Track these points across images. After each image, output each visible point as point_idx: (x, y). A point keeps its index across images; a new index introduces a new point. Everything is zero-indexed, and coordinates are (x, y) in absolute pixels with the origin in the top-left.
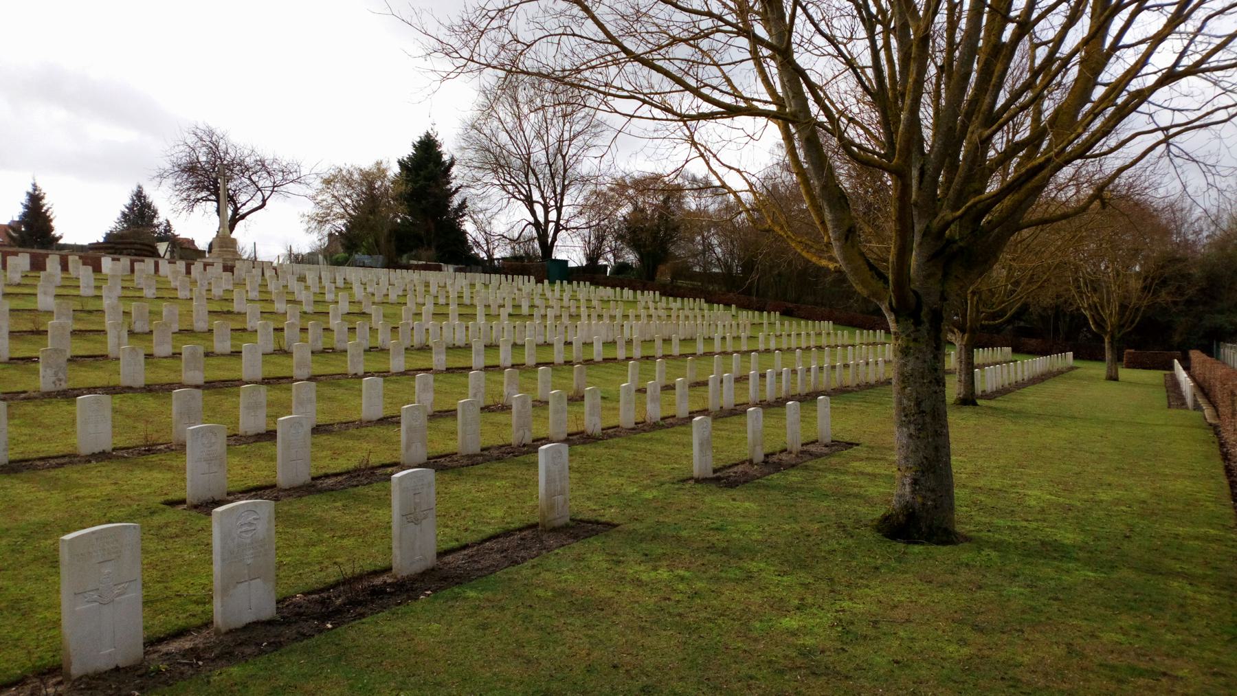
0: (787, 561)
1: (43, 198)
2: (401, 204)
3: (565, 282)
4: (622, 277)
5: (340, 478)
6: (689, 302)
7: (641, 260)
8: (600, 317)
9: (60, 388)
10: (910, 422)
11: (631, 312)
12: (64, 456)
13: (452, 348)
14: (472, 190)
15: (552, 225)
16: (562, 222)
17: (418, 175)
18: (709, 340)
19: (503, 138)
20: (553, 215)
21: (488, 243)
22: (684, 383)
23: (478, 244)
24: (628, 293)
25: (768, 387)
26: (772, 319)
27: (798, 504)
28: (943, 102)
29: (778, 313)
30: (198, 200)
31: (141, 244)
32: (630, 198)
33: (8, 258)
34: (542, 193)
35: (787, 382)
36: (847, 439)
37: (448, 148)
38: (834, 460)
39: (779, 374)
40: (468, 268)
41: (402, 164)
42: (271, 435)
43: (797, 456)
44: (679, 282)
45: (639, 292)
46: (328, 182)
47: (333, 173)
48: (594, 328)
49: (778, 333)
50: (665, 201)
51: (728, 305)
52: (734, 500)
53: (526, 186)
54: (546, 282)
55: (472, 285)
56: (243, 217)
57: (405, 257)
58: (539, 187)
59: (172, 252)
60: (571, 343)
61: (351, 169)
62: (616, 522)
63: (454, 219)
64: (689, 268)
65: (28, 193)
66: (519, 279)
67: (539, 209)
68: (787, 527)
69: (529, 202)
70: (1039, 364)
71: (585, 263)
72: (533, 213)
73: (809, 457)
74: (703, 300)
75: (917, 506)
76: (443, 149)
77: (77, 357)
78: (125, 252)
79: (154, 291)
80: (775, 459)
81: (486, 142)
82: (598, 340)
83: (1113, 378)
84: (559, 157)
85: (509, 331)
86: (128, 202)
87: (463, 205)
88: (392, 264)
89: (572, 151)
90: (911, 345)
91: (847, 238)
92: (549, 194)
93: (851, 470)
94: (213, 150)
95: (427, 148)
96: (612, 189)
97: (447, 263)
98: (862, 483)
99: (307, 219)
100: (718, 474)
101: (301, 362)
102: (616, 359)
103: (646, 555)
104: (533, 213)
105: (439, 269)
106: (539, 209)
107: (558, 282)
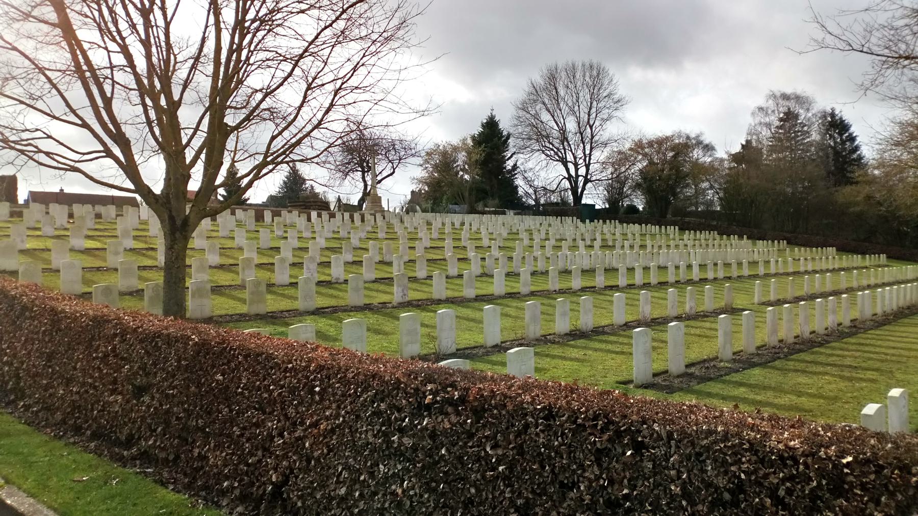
4: (631, 215)
6: (703, 236)
7: (648, 203)
20: (582, 171)
26: (781, 247)
28: (160, 140)
33: (356, 203)
37: (505, 125)
41: (473, 138)
47: (432, 147)
48: (671, 255)
49: (797, 258)
50: (675, 157)
58: (571, 151)
60: (633, 269)
61: (446, 145)
69: (565, 163)
72: (568, 170)
74: (716, 232)
76: (501, 126)
79: (365, 234)
82: (672, 265)
85: (616, 258)
87: (515, 167)
95: (491, 125)
96: (631, 149)
102: (707, 279)
104: (568, 170)
105: (504, 213)
107: (596, 221)
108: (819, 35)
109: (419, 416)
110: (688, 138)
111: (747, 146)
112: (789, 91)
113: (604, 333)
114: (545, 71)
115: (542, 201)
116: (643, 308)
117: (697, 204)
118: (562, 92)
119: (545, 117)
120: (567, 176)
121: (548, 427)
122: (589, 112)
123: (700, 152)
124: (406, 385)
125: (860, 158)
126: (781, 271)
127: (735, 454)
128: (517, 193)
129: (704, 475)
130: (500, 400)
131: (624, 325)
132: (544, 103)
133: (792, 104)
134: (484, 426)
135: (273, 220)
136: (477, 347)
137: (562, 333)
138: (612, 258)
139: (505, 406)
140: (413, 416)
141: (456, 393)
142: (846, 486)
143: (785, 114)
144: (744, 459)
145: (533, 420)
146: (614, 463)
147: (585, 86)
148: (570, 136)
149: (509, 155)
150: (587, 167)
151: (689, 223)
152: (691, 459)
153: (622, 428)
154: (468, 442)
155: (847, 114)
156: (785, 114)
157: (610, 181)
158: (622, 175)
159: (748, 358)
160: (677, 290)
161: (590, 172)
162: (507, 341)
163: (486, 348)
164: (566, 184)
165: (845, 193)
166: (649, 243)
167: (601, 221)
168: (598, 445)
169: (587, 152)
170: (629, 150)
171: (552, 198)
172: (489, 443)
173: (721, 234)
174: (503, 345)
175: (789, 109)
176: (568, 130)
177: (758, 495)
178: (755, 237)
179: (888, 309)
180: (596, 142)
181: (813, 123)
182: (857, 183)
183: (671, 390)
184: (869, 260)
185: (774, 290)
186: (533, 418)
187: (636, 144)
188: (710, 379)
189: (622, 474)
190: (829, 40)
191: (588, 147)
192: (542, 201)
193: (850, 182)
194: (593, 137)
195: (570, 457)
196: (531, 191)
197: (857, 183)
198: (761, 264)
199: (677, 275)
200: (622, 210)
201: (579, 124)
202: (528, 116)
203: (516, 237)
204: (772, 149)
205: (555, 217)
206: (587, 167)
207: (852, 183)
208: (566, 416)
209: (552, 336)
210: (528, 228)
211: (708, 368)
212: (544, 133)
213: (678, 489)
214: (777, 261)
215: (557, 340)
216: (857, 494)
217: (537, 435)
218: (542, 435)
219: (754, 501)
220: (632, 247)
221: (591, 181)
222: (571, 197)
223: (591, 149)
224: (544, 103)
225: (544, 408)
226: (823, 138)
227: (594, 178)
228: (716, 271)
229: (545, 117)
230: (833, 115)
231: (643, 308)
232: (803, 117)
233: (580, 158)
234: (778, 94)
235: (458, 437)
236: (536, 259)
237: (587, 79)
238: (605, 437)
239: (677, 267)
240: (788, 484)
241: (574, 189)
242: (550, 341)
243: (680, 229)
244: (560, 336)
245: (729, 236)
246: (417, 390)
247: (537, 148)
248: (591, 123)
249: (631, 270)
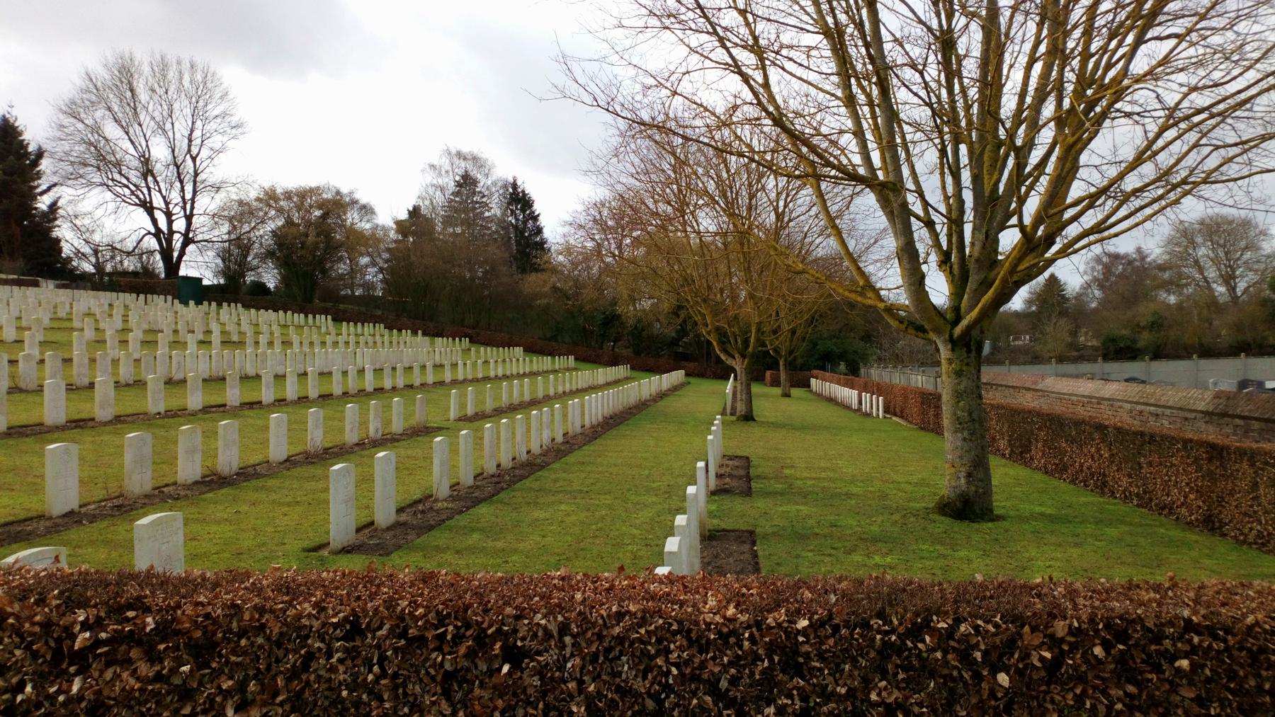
4: (258, 297)
6: (368, 328)
7: (285, 280)
8: (336, 344)
10: (963, 428)
13: (245, 378)
20: (179, 225)
40: (74, 285)
48: (330, 356)
50: (325, 216)
58: (160, 191)
69: (149, 209)
70: (650, 384)
72: (154, 222)
75: (971, 494)
76: (26, 136)
82: (338, 369)
83: (787, 395)
87: (53, 207)
90: (964, 368)
96: (258, 199)
102: (382, 389)
104: (154, 222)
105: (36, 284)
107: (205, 303)
108: (562, 80)
109: (57, 677)
110: (338, 193)
111: (415, 212)
112: (465, 149)
113: (257, 476)
114: (111, 59)
115: (109, 268)
116: (312, 434)
117: (352, 287)
118: (143, 96)
119: (112, 131)
120: (153, 231)
121: (352, 654)
122: (190, 135)
123: (356, 216)
124: (17, 617)
125: (543, 242)
126: (470, 377)
127: (659, 641)
128: (60, 250)
129: (618, 680)
130: (252, 619)
131: (286, 461)
132: (109, 109)
133: (469, 166)
134: (216, 674)
136: (31, 519)
137: (190, 482)
138: (245, 361)
139: (262, 627)
140: (41, 680)
141: (149, 620)
142: (801, 660)
143: (463, 177)
144: (672, 646)
145: (322, 645)
146: (477, 691)
147: (183, 94)
148: (158, 168)
149: (44, 187)
150: (189, 218)
151: (345, 311)
152: (598, 659)
153: (490, 632)
154: (181, 708)
155: (531, 187)
156: (463, 177)
157: (227, 244)
158: (244, 237)
159: (467, 493)
160: (357, 406)
161: (193, 227)
162: (89, 504)
163: (50, 518)
164: (152, 243)
165: (532, 282)
166: (295, 339)
167: (214, 304)
168: (448, 666)
169: (188, 196)
170: (256, 200)
171: (126, 263)
172: (230, 702)
173: (390, 328)
174: (83, 510)
175: (466, 172)
176: (153, 158)
177: (694, 694)
178: (434, 332)
179: (594, 422)
180: (203, 182)
181: (492, 194)
182: (543, 270)
183: (384, 550)
184: (560, 362)
185: (471, 400)
186: (323, 641)
187: (266, 193)
188: (431, 528)
189: (491, 705)
190: (573, 88)
191: (189, 188)
192: (109, 268)
193: (537, 269)
194: (196, 174)
195: (397, 697)
196: (87, 250)
197: (543, 270)
198: (447, 368)
199: (345, 383)
200: (244, 289)
201: (173, 151)
202: (80, 126)
203: (68, 324)
204: (447, 221)
205: (134, 295)
206: (189, 218)
207: (537, 270)
208: (387, 627)
209: (171, 488)
210: (87, 311)
211: (423, 512)
212: (110, 158)
213: (583, 709)
214: (465, 364)
215: (182, 493)
216: (814, 668)
217: (333, 669)
218: (341, 669)
219: (690, 704)
220: (271, 344)
221: (194, 242)
222: (161, 264)
223: (195, 192)
224: (109, 109)
225: (346, 619)
226: (504, 214)
227: (199, 237)
228: (394, 377)
229: (112, 131)
230: (515, 186)
231: (312, 434)
232: (482, 184)
233: (176, 205)
234: (454, 152)
235: (157, 703)
236: (116, 362)
237: (186, 82)
238: (462, 650)
239: (345, 373)
240: (733, 671)
241: (166, 253)
242: (170, 497)
243: (334, 320)
244: (187, 487)
245: (400, 330)
246: (47, 625)
247: (97, 179)
248: (194, 151)
249: (280, 378)
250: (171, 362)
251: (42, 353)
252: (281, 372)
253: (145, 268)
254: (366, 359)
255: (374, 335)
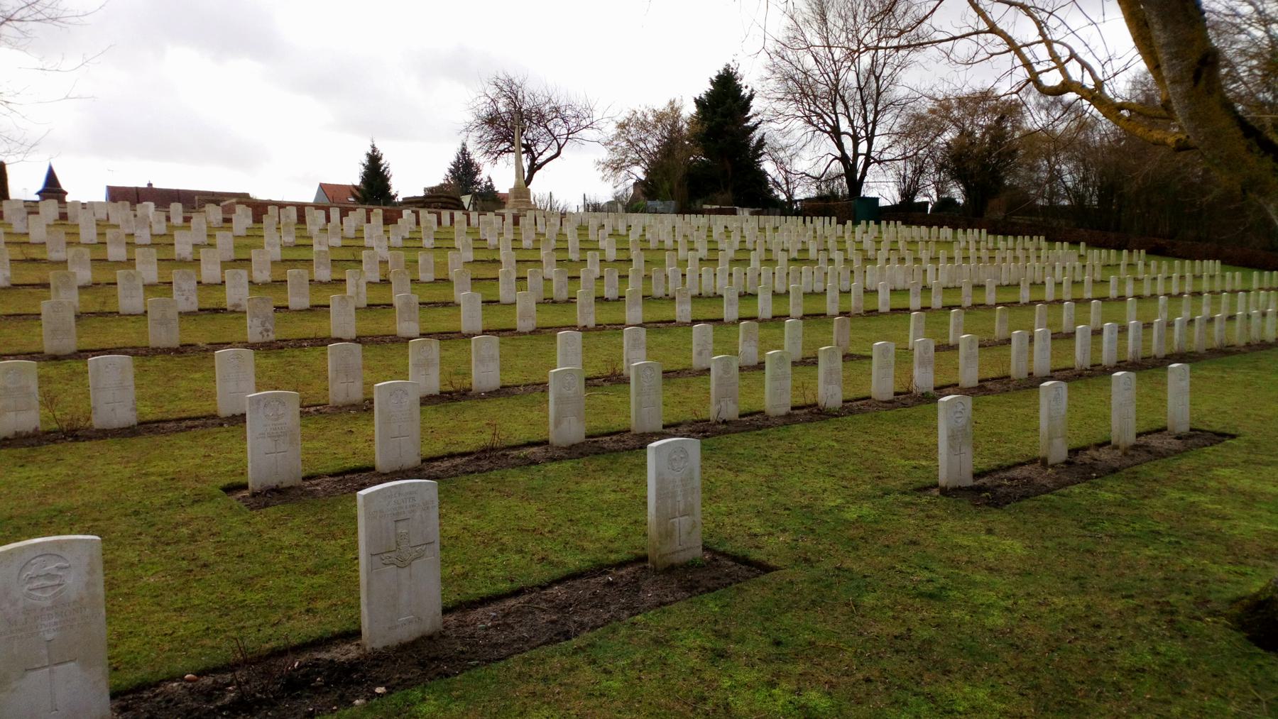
0: (1037, 687)
1: (380, 159)
2: (697, 146)
3: (872, 223)
4: (945, 214)
5: (458, 461)
9: (268, 339)
11: (943, 254)
12: (198, 418)
13: (1033, 284)
14: (772, 125)
15: (861, 159)
16: (873, 154)
17: (715, 113)
18: (1037, 285)
19: (809, 62)
20: (863, 147)
21: (787, 183)
22: (972, 341)
23: (778, 185)
24: (946, 232)
25: (1105, 346)
27: (1100, 549)
29: (1143, 252)
30: (501, 152)
31: (447, 197)
32: (955, 122)
34: (851, 122)
35: (1134, 340)
36: (1217, 426)
37: (751, 78)
38: (1186, 463)
39: (1097, 333)
40: (766, 211)
41: (699, 102)
42: (366, 407)
43: (1125, 454)
44: (1015, 219)
45: (960, 231)
46: (622, 126)
51: (1074, 243)
52: (990, 531)
53: (833, 116)
54: (849, 223)
55: (762, 230)
56: (540, 167)
57: (698, 203)
58: (849, 117)
59: (475, 204)
61: (646, 111)
62: (772, 563)
63: (753, 159)
64: (1026, 198)
65: (368, 154)
66: (818, 221)
67: (848, 143)
68: (1059, 601)
69: (836, 133)
71: (898, 200)
72: (840, 146)
73: (1144, 456)
74: (1042, 238)
76: (743, 83)
77: (317, 306)
78: (432, 205)
80: (1085, 458)
81: (788, 67)
82: (885, 286)
84: (873, 78)
86: (453, 159)
87: (761, 143)
88: (683, 210)
89: (887, 71)
91: (1197, 78)
92: (859, 122)
93: (1213, 484)
94: (513, 97)
96: (933, 111)
97: (743, 206)
98: (1228, 510)
99: (602, 166)
100: (981, 481)
101: (795, 307)
103: (777, 643)
104: (840, 146)
105: (734, 212)
106: (848, 143)
107: (863, 222)
135: (342, 223)
151: (1014, 224)
223: (877, 113)
248: (878, 71)
250: (745, 279)
251: (602, 270)
252: (846, 288)
253: (832, 192)
254: (1034, 269)
255: (1014, 249)
